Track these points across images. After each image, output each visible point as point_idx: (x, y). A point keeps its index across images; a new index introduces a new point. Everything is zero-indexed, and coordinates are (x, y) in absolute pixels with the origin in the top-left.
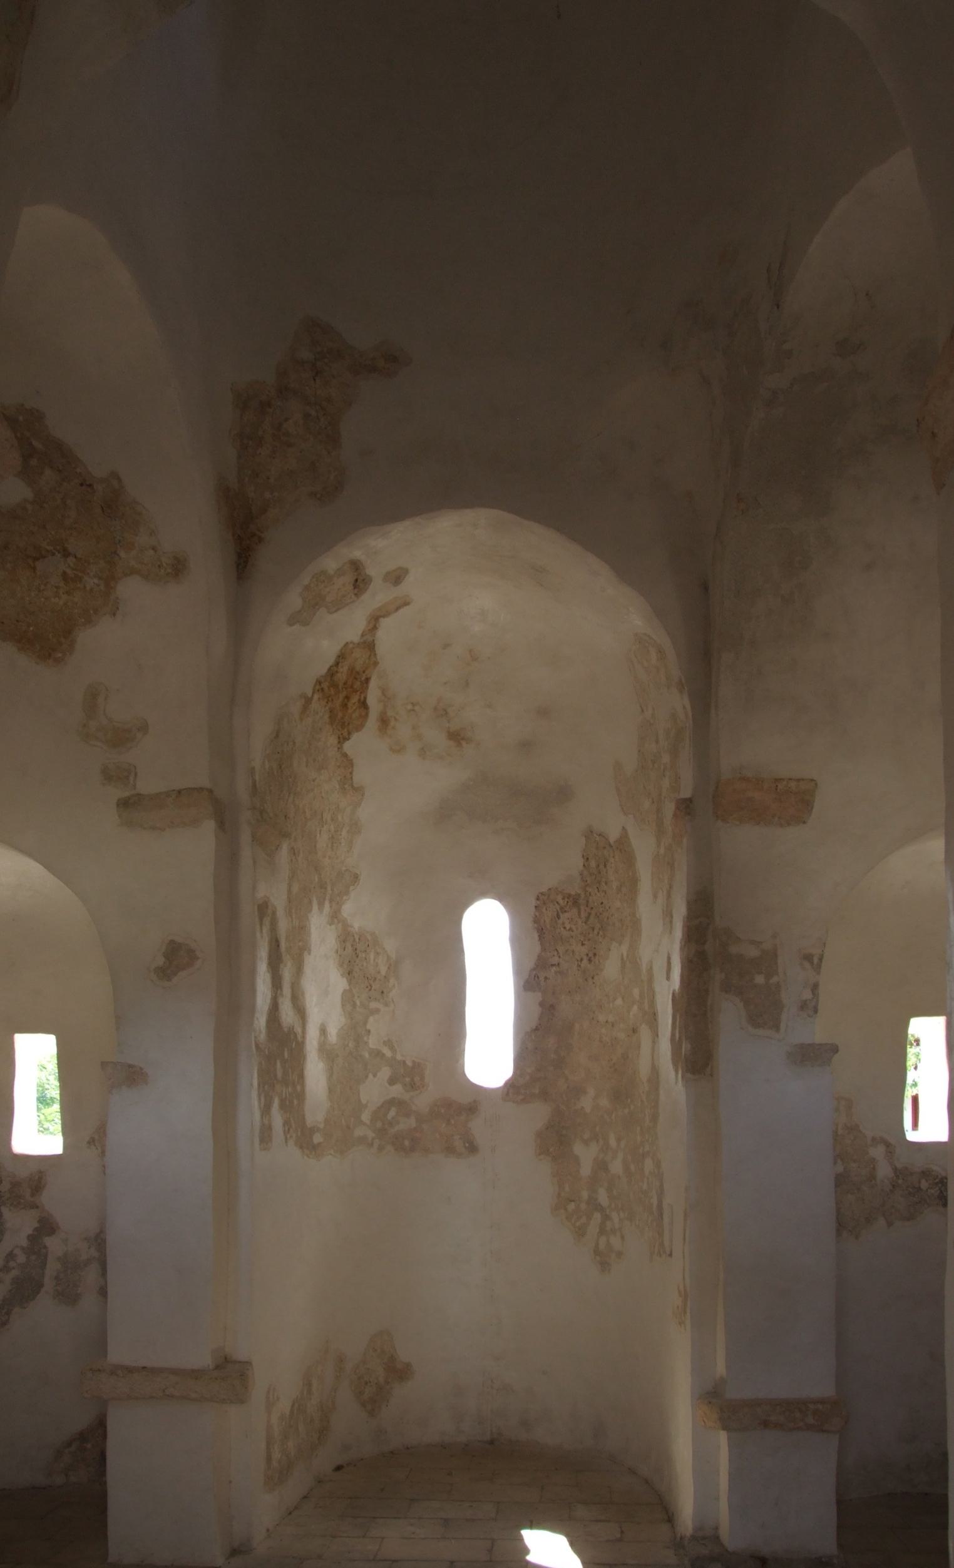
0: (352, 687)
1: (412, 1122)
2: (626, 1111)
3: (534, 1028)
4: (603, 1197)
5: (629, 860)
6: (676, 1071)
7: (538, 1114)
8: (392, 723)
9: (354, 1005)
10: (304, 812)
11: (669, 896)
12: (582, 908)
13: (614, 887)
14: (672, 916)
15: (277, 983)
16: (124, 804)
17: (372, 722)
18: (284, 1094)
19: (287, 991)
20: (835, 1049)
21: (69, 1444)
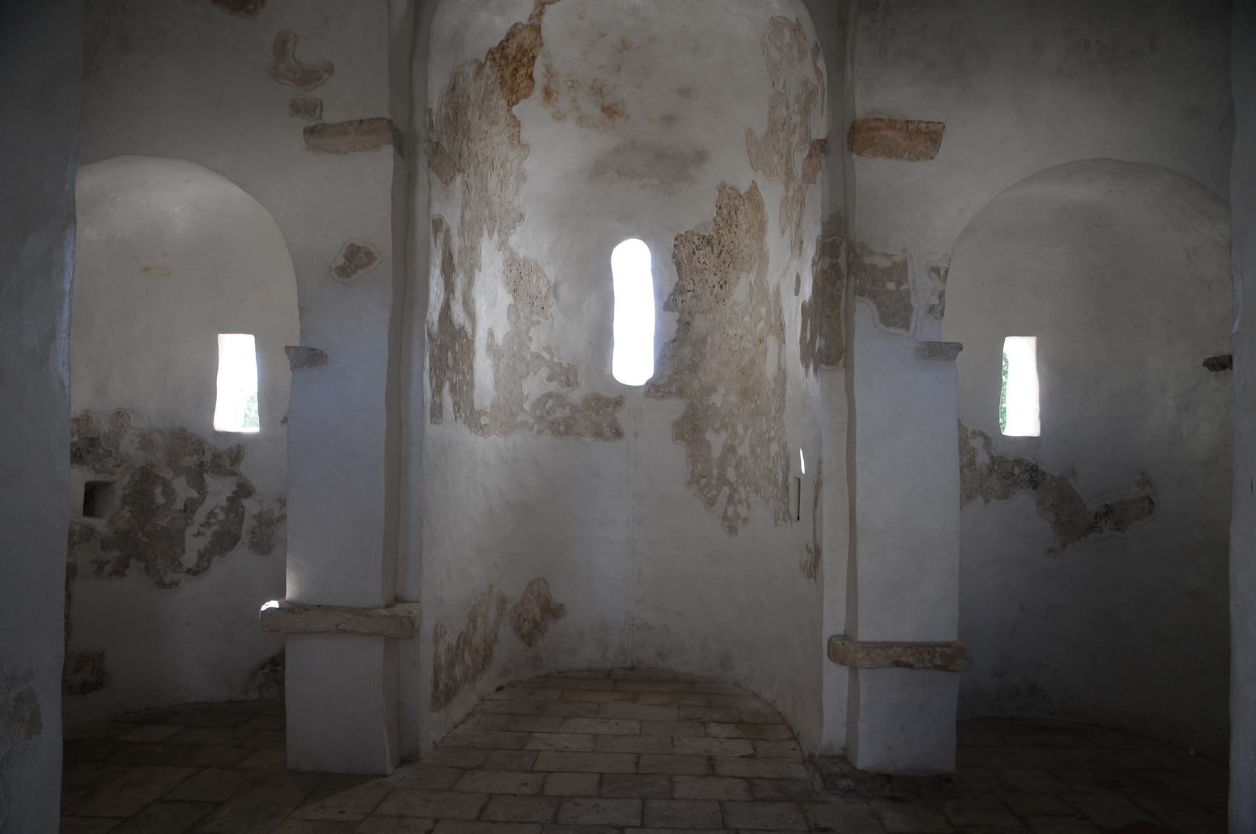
0: (520, 61)
1: (567, 411)
2: (753, 405)
3: (672, 339)
4: (731, 475)
5: (758, 206)
6: (807, 367)
7: (675, 407)
8: (555, 95)
9: (519, 316)
10: (477, 156)
11: (798, 226)
12: (715, 248)
13: (744, 229)
14: (802, 243)
15: (449, 288)
16: (310, 131)
17: (537, 93)
18: (454, 381)
19: (458, 294)
20: (959, 347)
21: (263, 668)
